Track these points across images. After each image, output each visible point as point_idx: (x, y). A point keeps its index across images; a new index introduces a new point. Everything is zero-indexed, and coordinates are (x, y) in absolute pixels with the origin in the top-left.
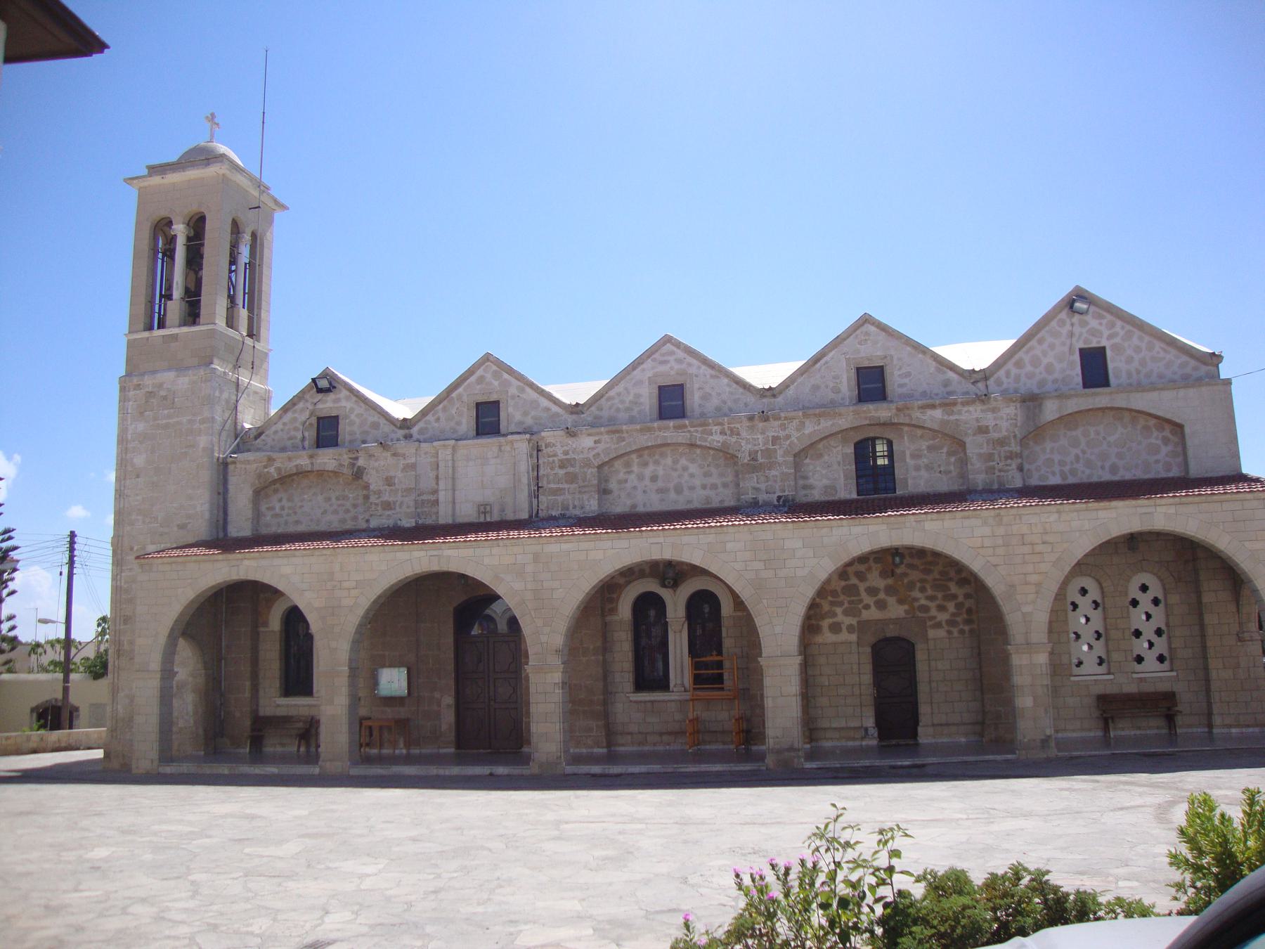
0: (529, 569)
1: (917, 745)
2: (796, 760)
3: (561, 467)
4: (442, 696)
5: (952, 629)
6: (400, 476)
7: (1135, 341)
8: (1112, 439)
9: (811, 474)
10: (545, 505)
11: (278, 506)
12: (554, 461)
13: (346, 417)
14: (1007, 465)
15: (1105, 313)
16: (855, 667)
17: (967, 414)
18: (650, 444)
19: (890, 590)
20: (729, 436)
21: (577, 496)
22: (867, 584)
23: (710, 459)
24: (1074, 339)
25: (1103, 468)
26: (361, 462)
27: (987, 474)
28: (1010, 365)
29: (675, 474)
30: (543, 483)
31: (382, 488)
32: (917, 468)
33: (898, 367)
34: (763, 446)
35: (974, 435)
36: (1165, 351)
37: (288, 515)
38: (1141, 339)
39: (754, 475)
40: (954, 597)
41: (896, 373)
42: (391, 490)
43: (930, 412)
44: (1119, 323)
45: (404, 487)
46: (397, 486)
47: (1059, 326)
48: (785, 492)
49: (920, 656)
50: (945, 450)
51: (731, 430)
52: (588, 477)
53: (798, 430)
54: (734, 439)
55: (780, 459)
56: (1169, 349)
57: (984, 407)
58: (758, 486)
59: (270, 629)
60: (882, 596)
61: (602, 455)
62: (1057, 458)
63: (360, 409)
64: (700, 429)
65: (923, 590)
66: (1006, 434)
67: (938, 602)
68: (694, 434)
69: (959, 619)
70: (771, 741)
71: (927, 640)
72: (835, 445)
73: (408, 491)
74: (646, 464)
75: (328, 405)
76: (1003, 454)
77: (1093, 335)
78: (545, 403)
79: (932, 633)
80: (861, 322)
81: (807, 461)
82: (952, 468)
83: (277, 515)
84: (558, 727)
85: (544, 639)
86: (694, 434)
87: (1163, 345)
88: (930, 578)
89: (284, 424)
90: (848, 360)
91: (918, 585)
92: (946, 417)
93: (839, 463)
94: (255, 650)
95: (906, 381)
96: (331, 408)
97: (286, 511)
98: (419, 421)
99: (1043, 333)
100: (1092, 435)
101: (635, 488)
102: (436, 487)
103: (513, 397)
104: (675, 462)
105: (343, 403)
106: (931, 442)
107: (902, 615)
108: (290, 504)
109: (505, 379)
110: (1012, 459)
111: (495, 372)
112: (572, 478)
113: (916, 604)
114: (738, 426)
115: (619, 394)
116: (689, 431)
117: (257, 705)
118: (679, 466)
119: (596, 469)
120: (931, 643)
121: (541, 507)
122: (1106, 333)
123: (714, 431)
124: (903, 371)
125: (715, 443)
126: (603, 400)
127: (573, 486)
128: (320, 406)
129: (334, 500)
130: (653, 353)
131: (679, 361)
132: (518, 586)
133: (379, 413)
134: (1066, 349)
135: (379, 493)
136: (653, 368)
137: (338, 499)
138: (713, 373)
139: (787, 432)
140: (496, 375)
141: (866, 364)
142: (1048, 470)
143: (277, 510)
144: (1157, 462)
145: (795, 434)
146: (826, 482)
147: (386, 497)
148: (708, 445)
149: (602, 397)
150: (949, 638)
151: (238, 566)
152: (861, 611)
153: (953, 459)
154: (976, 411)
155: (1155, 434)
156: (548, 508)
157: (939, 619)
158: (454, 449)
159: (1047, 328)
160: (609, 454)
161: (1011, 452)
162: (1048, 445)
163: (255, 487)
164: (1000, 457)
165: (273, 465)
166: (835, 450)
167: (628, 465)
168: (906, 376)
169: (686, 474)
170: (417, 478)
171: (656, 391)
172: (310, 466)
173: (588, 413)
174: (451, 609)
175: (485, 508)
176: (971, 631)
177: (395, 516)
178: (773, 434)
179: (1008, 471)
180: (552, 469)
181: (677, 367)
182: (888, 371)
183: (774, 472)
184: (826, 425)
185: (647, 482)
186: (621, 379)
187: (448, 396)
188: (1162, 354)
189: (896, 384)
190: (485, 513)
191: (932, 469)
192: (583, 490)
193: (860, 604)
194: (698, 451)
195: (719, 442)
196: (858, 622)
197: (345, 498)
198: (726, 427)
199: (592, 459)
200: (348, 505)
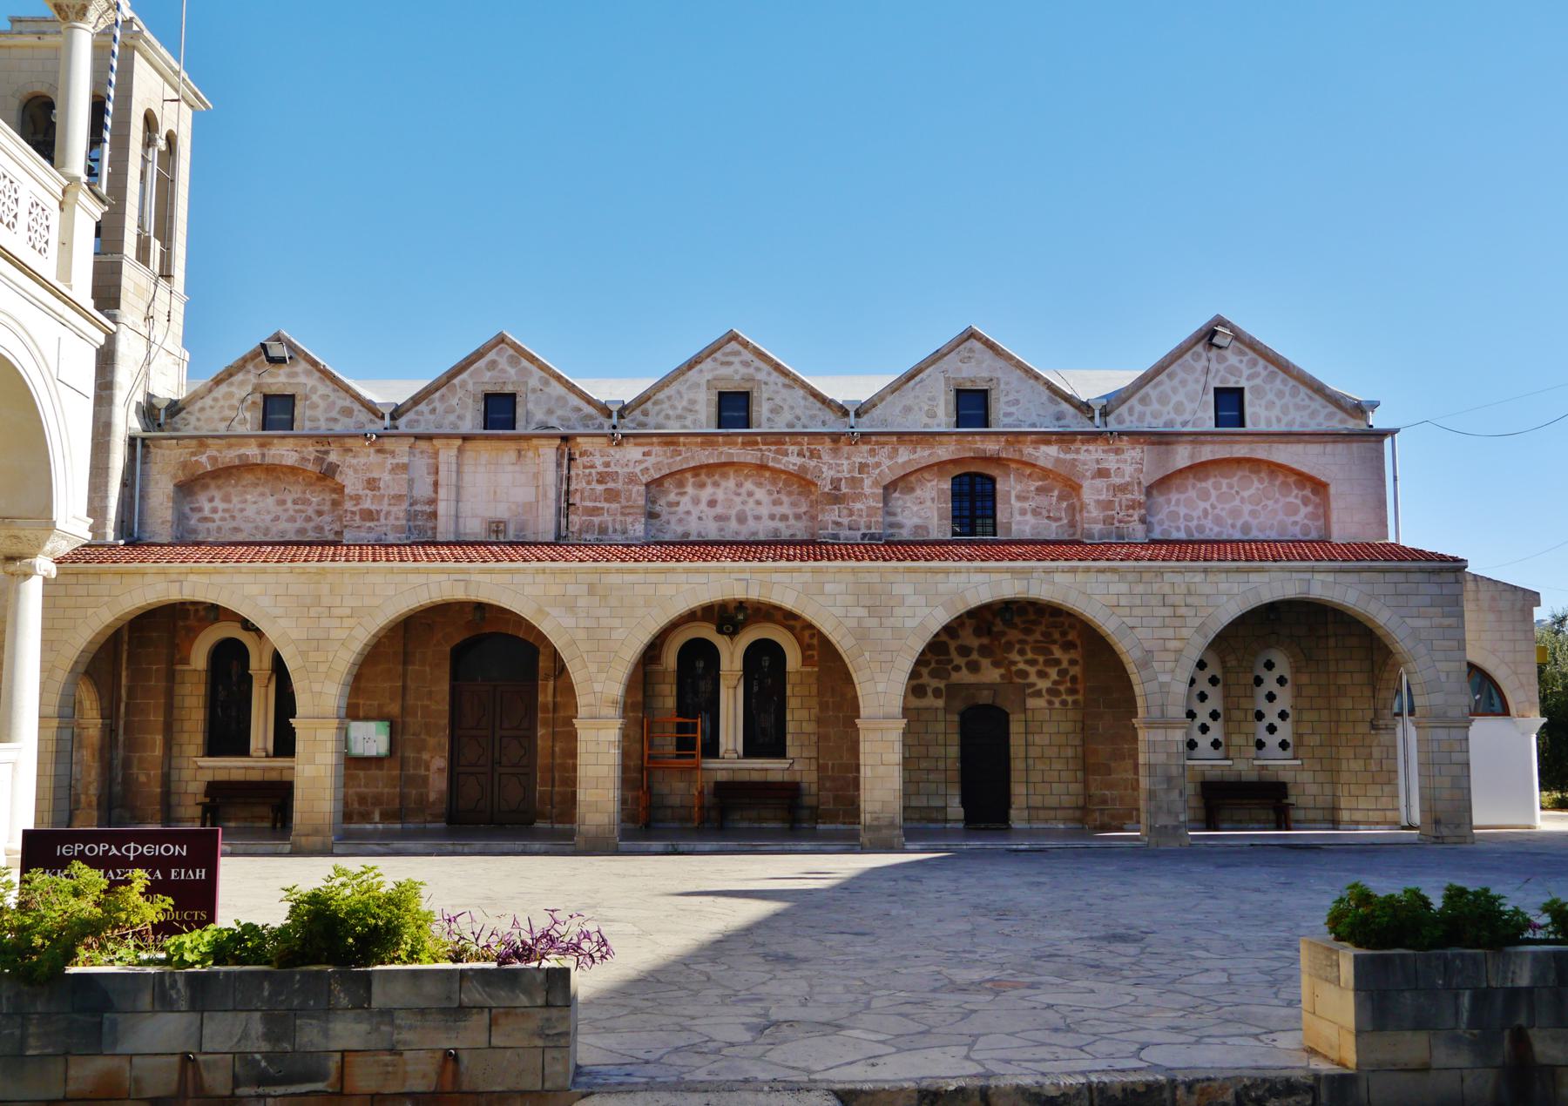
0: (582, 602)
1: (1009, 828)
2: (896, 840)
3: (599, 482)
4: (432, 757)
5: (1053, 699)
6: (387, 478)
7: (1278, 383)
8: (1246, 494)
9: (900, 510)
10: (577, 527)
11: (207, 507)
12: (590, 474)
13: (306, 398)
14: (1128, 516)
15: (1247, 350)
16: (941, 737)
17: (1086, 454)
18: (712, 461)
19: (984, 651)
20: (809, 459)
21: (619, 518)
22: (960, 642)
23: (781, 485)
24: (1210, 376)
25: (1233, 526)
26: (333, 457)
27: (1104, 524)
28: (1134, 401)
29: (738, 500)
30: (575, 499)
31: (360, 492)
32: (1023, 512)
33: (1004, 393)
34: (849, 472)
35: (1093, 478)
36: (1311, 398)
37: (224, 519)
38: (1284, 382)
39: (836, 507)
40: (1057, 662)
41: (1003, 399)
42: (374, 496)
43: (1043, 448)
44: (1262, 362)
45: (392, 493)
46: (382, 491)
47: (1194, 360)
48: (870, 529)
49: (1016, 727)
50: (1056, 493)
51: (811, 452)
52: (633, 495)
53: (891, 458)
54: (813, 463)
55: (867, 491)
56: (1316, 397)
57: (1106, 448)
58: (840, 520)
59: (193, 667)
60: (975, 656)
61: (652, 471)
62: (1182, 511)
63: (325, 389)
64: (773, 448)
65: (1022, 652)
66: (1129, 479)
67: (1039, 667)
68: (766, 453)
69: (1062, 688)
70: (868, 816)
71: (1025, 710)
72: (930, 478)
73: (398, 498)
74: (702, 485)
75: (278, 381)
76: (1124, 503)
77: (1231, 374)
78: (575, 401)
79: (1032, 703)
80: (965, 336)
81: (896, 495)
82: (1063, 515)
83: (205, 519)
84: (611, 795)
85: (597, 687)
86: (766, 453)
87: (1309, 392)
88: (1030, 639)
89: (215, 400)
90: (947, 379)
91: (1017, 646)
92: (1062, 456)
93: (933, 499)
94: (170, 694)
95: (1013, 409)
96: (284, 384)
97: (220, 514)
98: (408, 411)
99: (1174, 367)
100: (1224, 489)
101: (688, 513)
102: (433, 495)
103: (534, 391)
104: (740, 485)
105: (302, 379)
106: (1040, 483)
107: (998, 680)
108: (225, 506)
109: (525, 369)
110: (1134, 509)
111: (511, 356)
112: (612, 495)
113: (1014, 668)
114: (819, 447)
115: (669, 398)
116: (761, 450)
117: (170, 768)
118: (743, 491)
119: (644, 487)
120: (1030, 713)
121: (571, 529)
122: (1246, 372)
123: (790, 451)
124: (1011, 397)
125: (791, 466)
126: (649, 404)
127: (614, 506)
128: (267, 379)
129: (289, 504)
130: (714, 351)
131: (746, 364)
132: (569, 622)
133: (353, 396)
134: (1200, 388)
135: (357, 499)
136: (712, 370)
137: (295, 502)
138: (787, 381)
139: (876, 459)
140: (513, 361)
141: (968, 386)
142: (1172, 524)
143: (207, 513)
144: (1295, 523)
145: (887, 463)
146: (916, 521)
147: (367, 504)
148: (783, 468)
149: (649, 398)
150: (1050, 710)
151: (181, 581)
152: (950, 674)
153: (1064, 504)
154: (1096, 451)
155: (1295, 492)
156: (580, 531)
157: (1038, 687)
158: (460, 450)
159: (1180, 361)
160: (660, 469)
161: (1133, 501)
162: (1174, 496)
163: (178, 480)
164: (1121, 506)
165: (204, 453)
166: (929, 485)
167: (681, 484)
168: (1014, 405)
169: (751, 501)
170: (411, 482)
171: (715, 398)
172: (259, 458)
173: (630, 417)
174: (448, 649)
175: (498, 527)
176: (1075, 702)
177: (379, 529)
178: (860, 460)
179: (1129, 522)
180: (589, 483)
181: (743, 370)
182: (993, 396)
183: (858, 506)
184: (923, 455)
185: (703, 506)
186: (675, 379)
187: (448, 382)
188: (1307, 402)
189: (1002, 412)
190: (497, 532)
191: (1040, 514)
192: (628, 511)
193: (949, 664)
194: (767, 474)
195: (795, 464)
196: (946, 686)
197: (307, 502)
198: (805, 448)
199: (639, 474)
200: (310, 511)
